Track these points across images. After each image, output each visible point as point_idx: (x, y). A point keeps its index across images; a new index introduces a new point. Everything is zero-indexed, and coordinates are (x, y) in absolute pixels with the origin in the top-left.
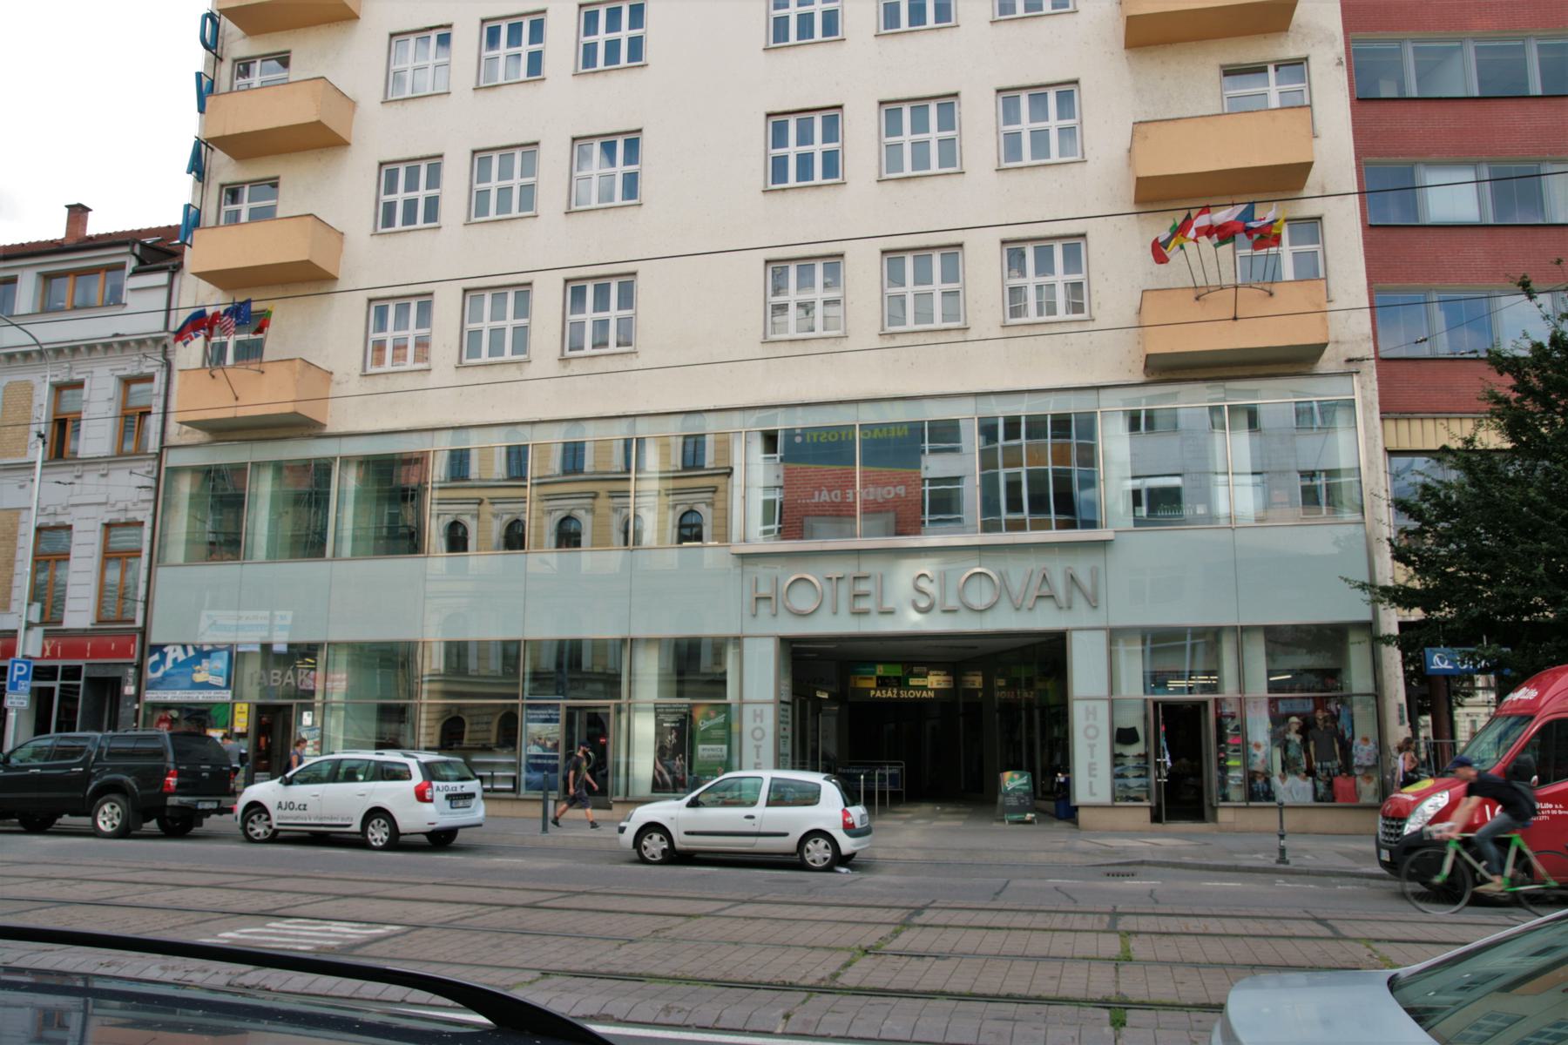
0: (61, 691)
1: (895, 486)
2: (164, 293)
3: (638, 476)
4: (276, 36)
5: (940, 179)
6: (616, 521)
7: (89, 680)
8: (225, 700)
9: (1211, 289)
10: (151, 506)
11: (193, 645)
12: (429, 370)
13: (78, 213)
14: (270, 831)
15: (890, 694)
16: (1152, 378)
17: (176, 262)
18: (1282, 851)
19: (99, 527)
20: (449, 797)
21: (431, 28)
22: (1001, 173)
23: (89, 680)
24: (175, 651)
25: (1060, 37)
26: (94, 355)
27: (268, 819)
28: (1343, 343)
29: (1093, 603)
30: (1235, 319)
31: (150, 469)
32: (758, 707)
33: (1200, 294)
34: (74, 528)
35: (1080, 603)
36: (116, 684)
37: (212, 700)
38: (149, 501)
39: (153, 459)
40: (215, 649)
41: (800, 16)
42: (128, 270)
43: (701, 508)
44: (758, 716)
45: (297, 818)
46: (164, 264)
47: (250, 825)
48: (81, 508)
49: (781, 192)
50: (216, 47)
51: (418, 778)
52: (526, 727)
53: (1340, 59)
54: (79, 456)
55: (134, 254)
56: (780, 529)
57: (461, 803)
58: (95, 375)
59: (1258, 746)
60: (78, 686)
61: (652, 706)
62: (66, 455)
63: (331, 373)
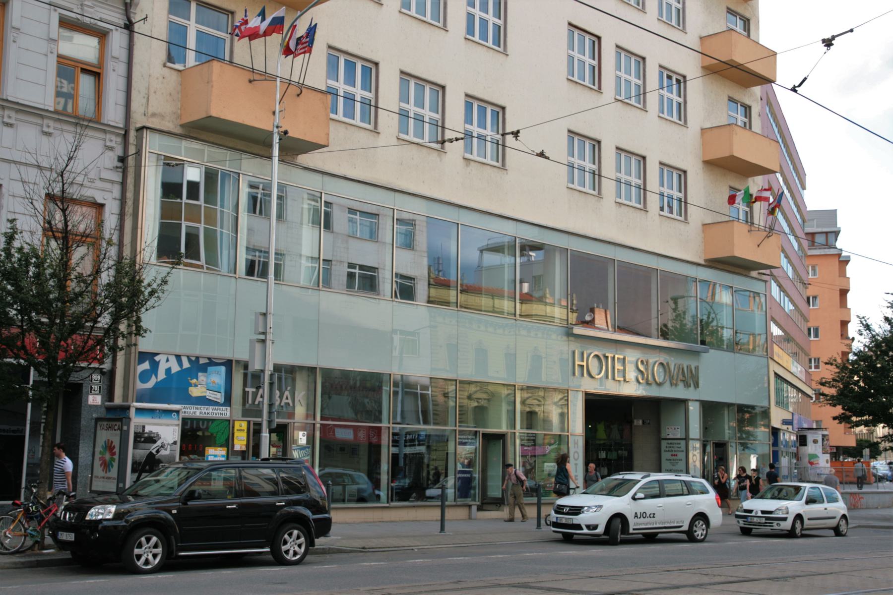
11: (188, 357)
24: (168, 360)
37: (210, 416)
39: (117, 135)
40: (212, 362)
49: (574, 84)
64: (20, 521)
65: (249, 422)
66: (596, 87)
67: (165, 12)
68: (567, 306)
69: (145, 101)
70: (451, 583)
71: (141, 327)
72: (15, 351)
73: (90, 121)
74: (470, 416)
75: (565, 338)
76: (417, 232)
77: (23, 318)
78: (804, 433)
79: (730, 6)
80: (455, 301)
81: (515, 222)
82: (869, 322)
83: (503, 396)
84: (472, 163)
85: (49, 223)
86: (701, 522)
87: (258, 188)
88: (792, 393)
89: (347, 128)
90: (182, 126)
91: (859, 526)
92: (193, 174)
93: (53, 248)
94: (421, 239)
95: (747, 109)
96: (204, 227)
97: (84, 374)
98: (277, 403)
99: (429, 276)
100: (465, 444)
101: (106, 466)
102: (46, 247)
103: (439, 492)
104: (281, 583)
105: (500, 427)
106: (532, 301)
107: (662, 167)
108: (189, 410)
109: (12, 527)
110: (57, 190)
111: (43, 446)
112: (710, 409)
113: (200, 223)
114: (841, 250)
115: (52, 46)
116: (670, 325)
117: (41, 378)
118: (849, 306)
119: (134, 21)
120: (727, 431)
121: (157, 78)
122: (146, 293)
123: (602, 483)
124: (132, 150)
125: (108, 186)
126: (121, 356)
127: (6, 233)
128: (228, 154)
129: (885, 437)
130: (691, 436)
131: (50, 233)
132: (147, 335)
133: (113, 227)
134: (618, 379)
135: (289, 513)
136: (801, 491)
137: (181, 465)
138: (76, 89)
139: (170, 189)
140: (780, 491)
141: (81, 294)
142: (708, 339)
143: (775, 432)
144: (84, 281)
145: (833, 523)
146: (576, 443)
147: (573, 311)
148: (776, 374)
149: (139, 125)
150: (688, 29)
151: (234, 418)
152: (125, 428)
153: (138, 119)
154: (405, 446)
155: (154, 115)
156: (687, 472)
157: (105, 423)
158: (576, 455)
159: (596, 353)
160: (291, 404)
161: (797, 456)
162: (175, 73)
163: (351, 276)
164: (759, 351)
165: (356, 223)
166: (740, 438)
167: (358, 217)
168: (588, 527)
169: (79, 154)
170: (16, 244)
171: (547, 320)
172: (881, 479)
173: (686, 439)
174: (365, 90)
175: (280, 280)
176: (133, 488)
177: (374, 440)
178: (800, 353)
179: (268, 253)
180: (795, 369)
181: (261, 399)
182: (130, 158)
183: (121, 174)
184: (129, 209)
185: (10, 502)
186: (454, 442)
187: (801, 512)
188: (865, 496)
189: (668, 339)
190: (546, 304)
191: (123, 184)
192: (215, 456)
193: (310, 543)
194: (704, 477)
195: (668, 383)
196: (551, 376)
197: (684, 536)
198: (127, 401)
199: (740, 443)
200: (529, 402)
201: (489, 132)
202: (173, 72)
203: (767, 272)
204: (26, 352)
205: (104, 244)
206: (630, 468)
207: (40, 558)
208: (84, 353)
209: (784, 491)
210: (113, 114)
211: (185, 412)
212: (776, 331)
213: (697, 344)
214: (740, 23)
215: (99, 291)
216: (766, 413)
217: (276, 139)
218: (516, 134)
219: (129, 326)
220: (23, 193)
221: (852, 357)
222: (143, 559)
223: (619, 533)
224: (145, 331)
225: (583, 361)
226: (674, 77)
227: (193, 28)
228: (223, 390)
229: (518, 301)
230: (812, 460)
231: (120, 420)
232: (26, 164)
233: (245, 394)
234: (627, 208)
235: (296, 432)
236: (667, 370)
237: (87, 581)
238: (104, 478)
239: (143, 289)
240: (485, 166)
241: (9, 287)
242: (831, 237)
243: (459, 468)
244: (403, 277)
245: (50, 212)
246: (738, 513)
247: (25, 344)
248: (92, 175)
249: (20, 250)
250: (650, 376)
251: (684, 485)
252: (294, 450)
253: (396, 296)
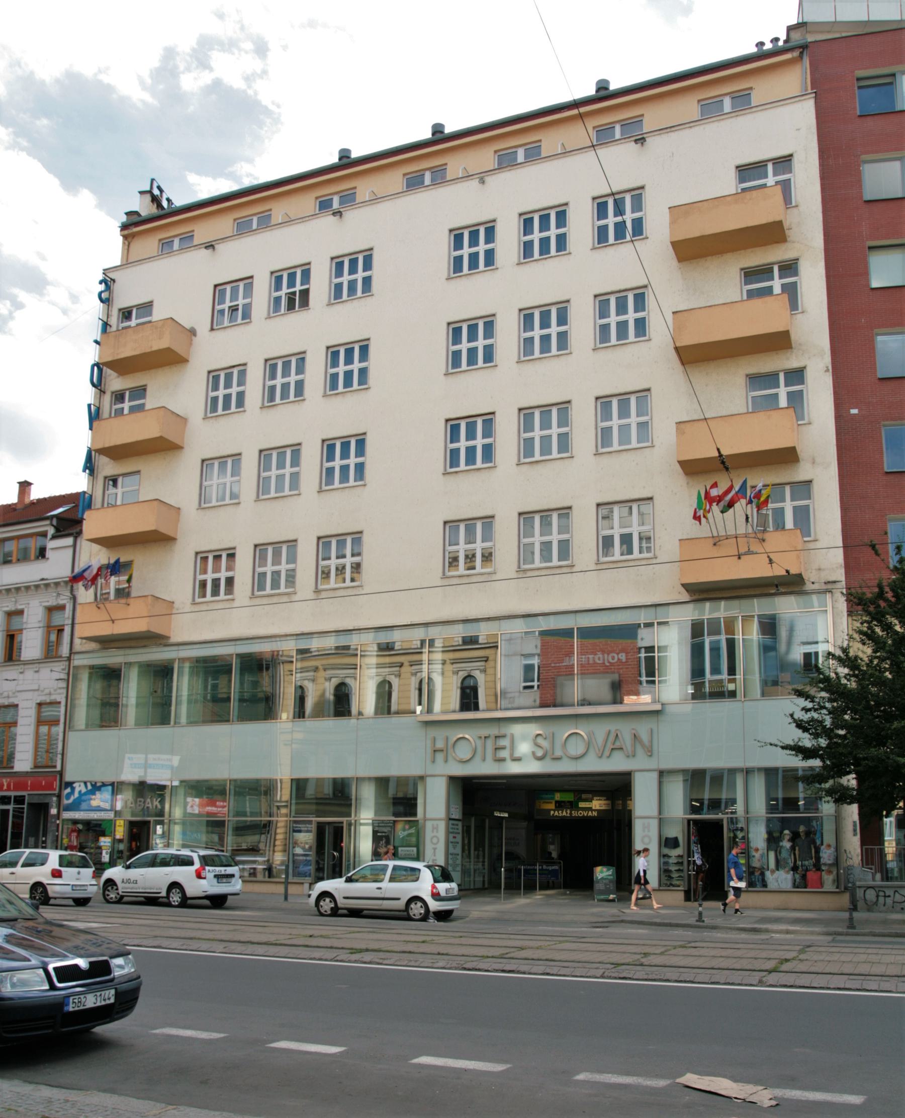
0: (14, 811)
1: (618, 654)
2: (71, 551)
3: (430, 650)
4: (139, 375)
5: (558, 462)
6: (414, 682)
7: (30, 804)
8: (109, 818)
9: (722, 538)
10: (65, 691)
12: (233, 600)
13: (25, 486)
14: (118, 897)
15: (565, 813)
16: (694, 598)
17: (78, 530)
18: (700, 914)
19: (34, 705)
20: (215, 876)
21: (234, 367)
22: (597, 456)
23: (30, 804)
25: (639, 358)
26: (30, 593)
27: (117, 889)
28: (824, 570)
29: (650, 752)
31: (64, 667)
32: (435, 823)
33: (716, 541)
34: (20, 706)
35: (640, 751)
36: (45, 807)
38: (63, 688)
40: (104, 785)
41: (469, 350)
42: (49, 536)
43: (477, 674)
44: (435, 828)
45: (132, 888)
46: (71, 532)
47: (107, 893)
48: (23, 693)
49: (455, 475)
50: (100, 385)
51: (197, 865)
52: (293, 836)
53: (827, 367)
54: (22, 659)
55: (53, 525)
56: (538, 686)
57: (224, 880)
58: (31, 605)
59: (757, 850)
60: (23, 808)
61: (370, 821)
62: (14, 658)
63: (173, 603)
192: (105, 842)
252: (639, 853)
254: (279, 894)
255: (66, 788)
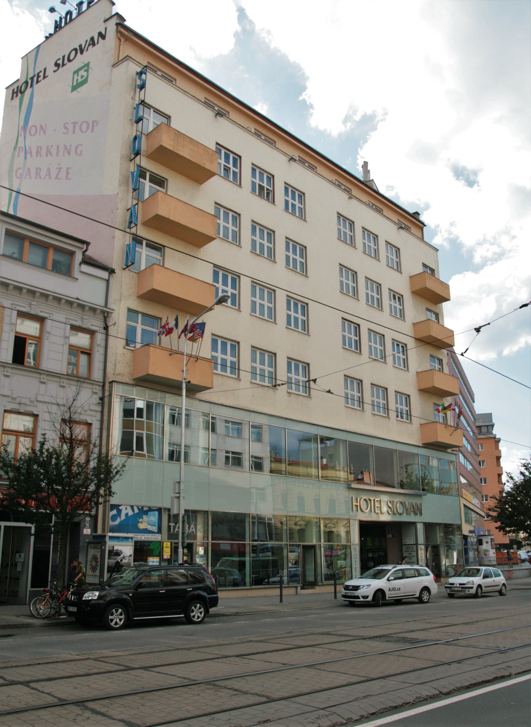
8: (157, 540)
11: (137, 507)
24: (126, 509)
30: (7, 350)
37: (150, 540)
39: (99, 385)
40: (150, 509)
45: (396, 594)
64: (47, 600)
65: (171, 543)
66: (358, 352)
67: (125, 320)
68: (348, 471)
69: (113, 367)
70: (286, 633)
71: (111, 491)
72: (45, 506)
73: (85, 379)
74: (296, 536)
75: (347, 490)
76: (263, 432)
77: (48, 487)
78: (481, 538)
79: (428, 307)
80: (285, 470)
81: (316, 427)
82: (512, 475)
83: (314, 523)
84: (292, 395)
85: (63, 435)
86: (426, 592)
87: (176, 410)
88: (474, 515)
89: (223, 378)
90: (133, 380)
91: (513, 589)
92: (140, 404)
93: (65, 449)
94: (266, 436)
95: (440, 361)
96: (146, 433)
97: (81, 518)
98: (187, 532)
99: (271, 457)
100: (293, 552)
101: (94, 569)
102: (61, 449)
103: (278, 579)
104: (191, 635)
105: (312, 542)
106: (327, 468)
107: (397, 393)
108: (138, 536)
109: (43, 603)
110: (67, 417)
111: (59, 558)
112: (429, 527)
113: (143, 430)
114: (495, 435)
115: (66, 340)
116: (405, 480)
117: (58, 520)
118: (501, 466)
119: (109, 325)
120: (439, 539)
121: (121, 355)
122: (114, 472)
123: (371, 571)
124: (107, 394)
125: (94, 413)
126: (101, 507)
127: (40, 442)
128: (159, 394)
129: (524, 538)
130: (419, 543)
131: (63, 440)
132: (115, 495)
133: (97, 435)
134: (377, 512)
135: (195, 595)
136: (481, 571)
137: (134, 568)
138: (78, 361)
139: (128, 413)
140: (469, 571)
141: (79, 474)
142: (426, 488)
143: (465, 537)
144: (81, 466)
145: (498, 588)
146: (355, 549)
147: (351, 473)
148: (465, 506)
149: (111, 380)
150: (406, 320)
151: (163, 540)
152: (103, 548)
153: (110, 377)
154: (260, 553)
155: (119, 374)
156: (418, 564)
157: (93, 545)
158: (355, 556)
159: (365, 498)
160: (195, 532)
161: (477, 550)
162: (130, 352)
163: (227, 458)
164: (454, 492)
165: (229, 428)
166: (446, 543)
167: (230, 425)
168: (363, 597)
169: (79, 398)
170: (46, 447)
171: (336, 480)
172: (523, 561)
173: (417, 544)
174: (232, 357)
175: (188, 463)
176: (108, 581)
177: (242, 550)
178: (477, 492)
179: (180, 445)
180: (475, 502)
181: (178, 530)
182: (106, 398)
183: (101, 407)
184: (105, 426)
185: (43, 589)
186: (286, 550)
187: (480, 583)
188: (515, 572)
189: (404, 489)
190: (336, 470)
191: (102, 412)
192: (153, 562)
193: (207, 611)
194: (427, 566)
195: (405, 513)
196: (341, 511)
197: (417, 600)
198: (104, 533)
199: (446, 545)
200: (328, 525)
201: (301, 378)
202: (129, 351)
203: (457, 449)
204: (51, 507)
205: (92, 446)
206: (386, 563)
207: (59, 621)
208: (81, 506)
209: (471, 572)
210: (97, 375)
211: (136, 538)
212: (463, 481)
213: (420, 491)
214: (434, 316)
215: (89, 472)
216: (459, 527)
217: (184, 385)
218: (315, 381)
219: (105, 491)
220: (49, 419)
221: (504, 495)
222: (114, 622)
223: (381, 600)
224: (114, 493)
225: (357, 502)
226: (400, 345)
227: (139, 327)
228: (157, 525)
229: (320, 469)
230: (486, 553)
231: (101, 543)
232: (51, 403)
233: (169, 527)
234: (379, 417)
235: (197, 547)
236: (404, 506)
237: (84, 634)
238: (92, 575)
239: (112, 470)
240: (299, 397)
241: (42, 470)
242: (490, 428)
243: (290, 565)
244: (256, 457)
245: (63, 429)
246: (446, 585)
247: (50, 502)
248: (85, 408)
249: (48, 450)
250: (395, 510)
251: (416, 571)
253: (252, 468)
254: (332, 593)
255: (112, 509)
